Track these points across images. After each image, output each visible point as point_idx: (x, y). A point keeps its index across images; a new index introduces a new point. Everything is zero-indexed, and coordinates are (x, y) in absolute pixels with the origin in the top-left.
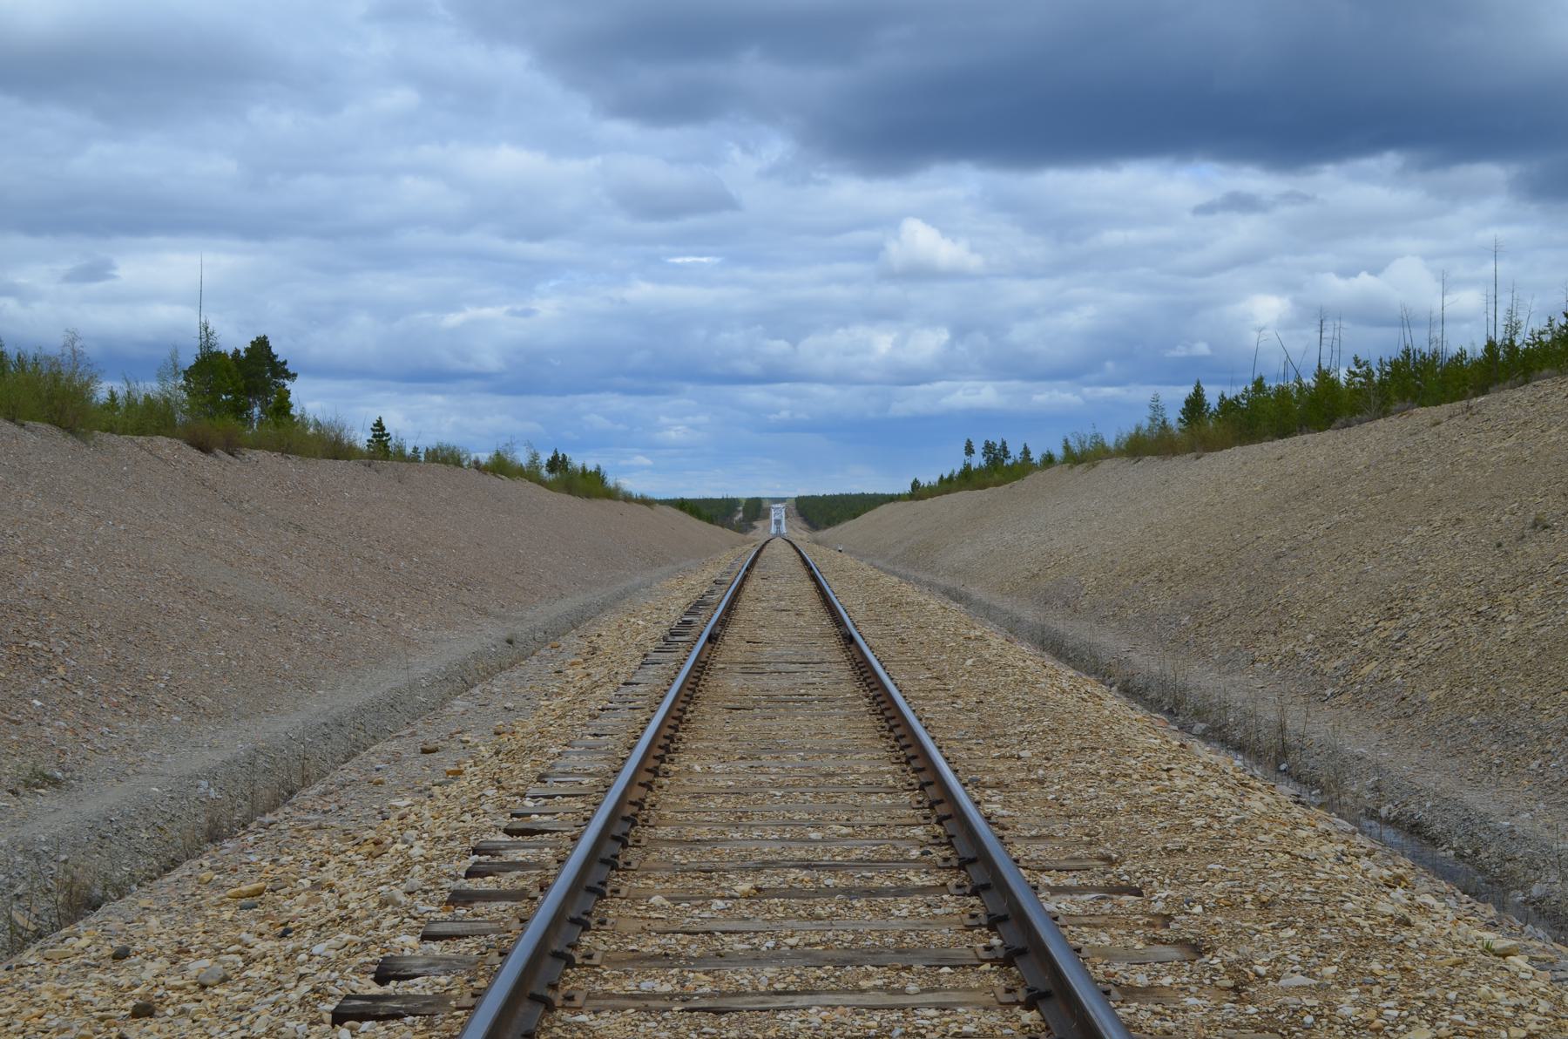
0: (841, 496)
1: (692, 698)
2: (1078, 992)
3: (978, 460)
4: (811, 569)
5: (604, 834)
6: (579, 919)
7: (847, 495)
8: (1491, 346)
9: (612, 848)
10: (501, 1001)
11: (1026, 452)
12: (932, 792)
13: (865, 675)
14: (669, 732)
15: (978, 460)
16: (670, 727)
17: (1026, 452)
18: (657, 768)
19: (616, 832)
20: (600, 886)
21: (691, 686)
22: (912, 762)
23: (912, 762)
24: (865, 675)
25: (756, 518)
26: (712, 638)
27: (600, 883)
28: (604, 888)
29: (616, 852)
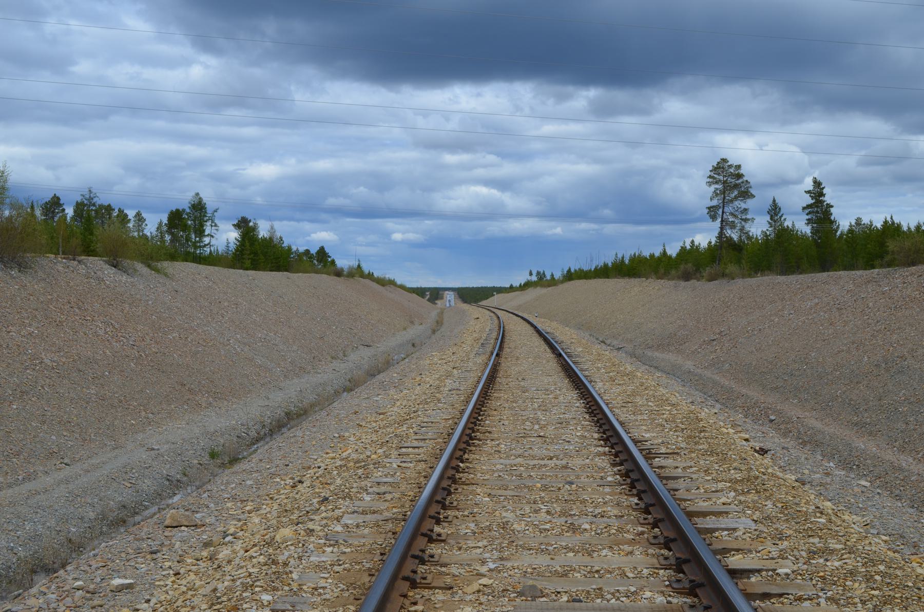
0: (482, 288)
1: (484, 403)
2: (643, 467)
3: (534, 278)
4: (560, 355)
5: (447, 467)
6: (434, 516)
7: (485, 288)
8: (886, 222)
9: (455, 463)
10: (389, 577)
11: (552, 275)
12: (618, 448)
13: (590, 404)
14: (471, 426)
15: (534, 278)
16: (472, 423)
17: (552, 275)
18: (462, 456)
19: (439, 498)
20: (436, 515)
21: (481, 403)
22: (603, 426)
23: (603, 426)
24: (590, 404)
25: (437, 299)
26: (497, 355)
27: (429, 530)
28: (432, 534)
29: (438, 511)
